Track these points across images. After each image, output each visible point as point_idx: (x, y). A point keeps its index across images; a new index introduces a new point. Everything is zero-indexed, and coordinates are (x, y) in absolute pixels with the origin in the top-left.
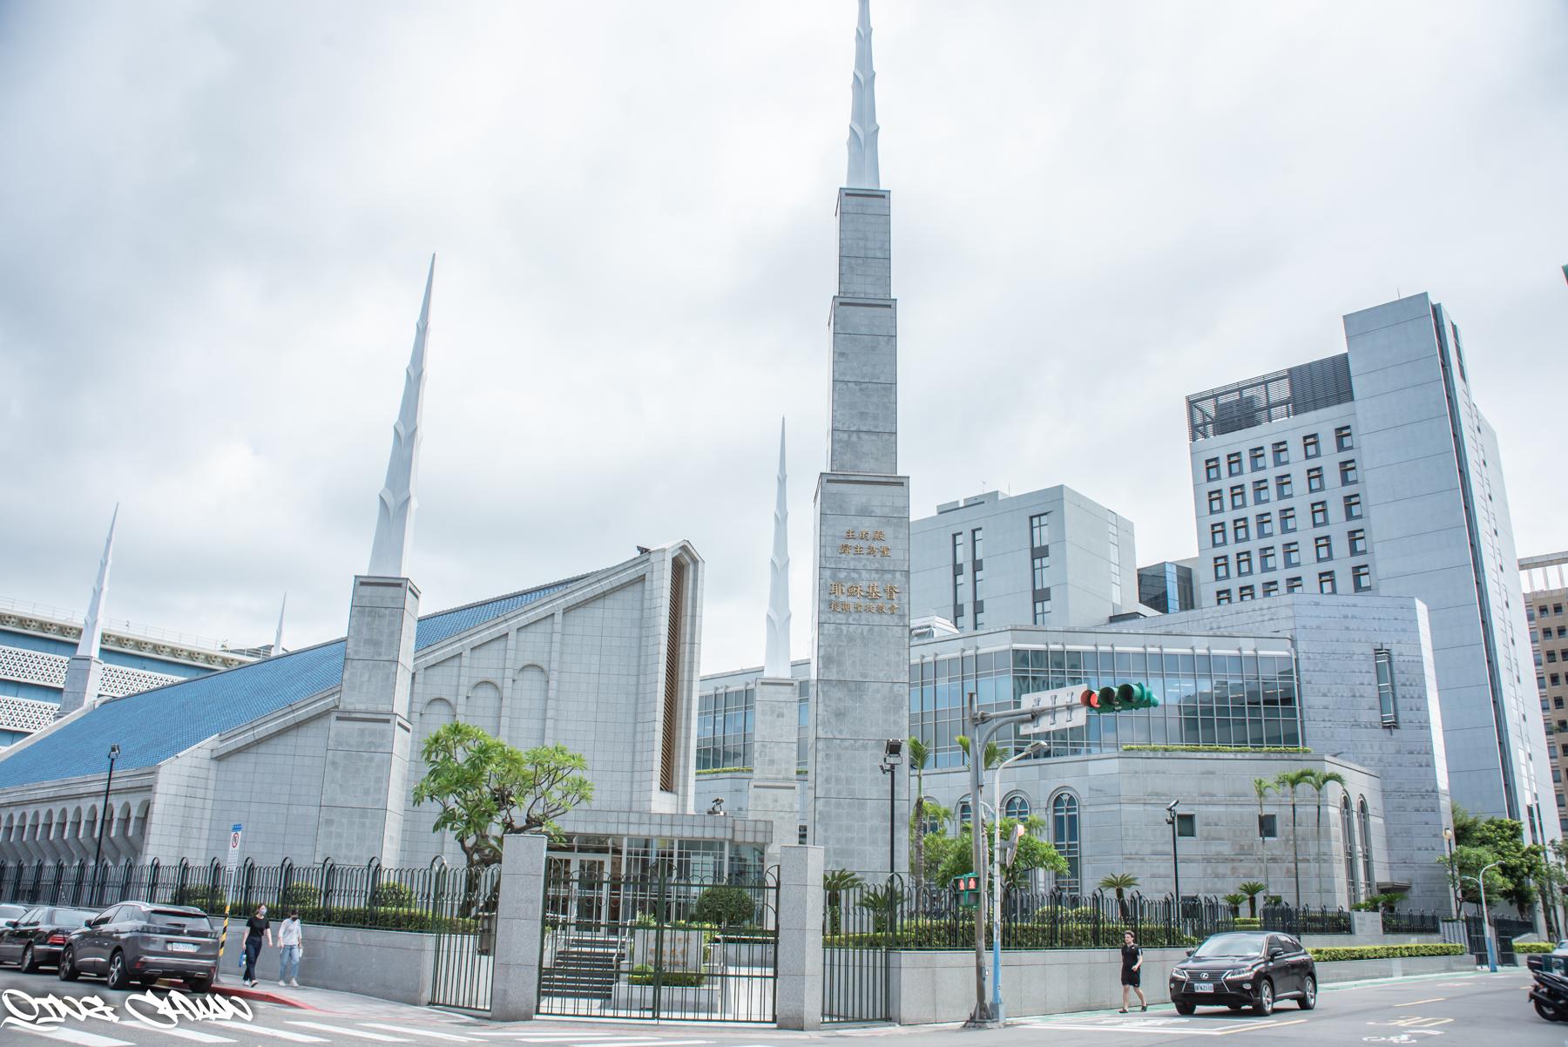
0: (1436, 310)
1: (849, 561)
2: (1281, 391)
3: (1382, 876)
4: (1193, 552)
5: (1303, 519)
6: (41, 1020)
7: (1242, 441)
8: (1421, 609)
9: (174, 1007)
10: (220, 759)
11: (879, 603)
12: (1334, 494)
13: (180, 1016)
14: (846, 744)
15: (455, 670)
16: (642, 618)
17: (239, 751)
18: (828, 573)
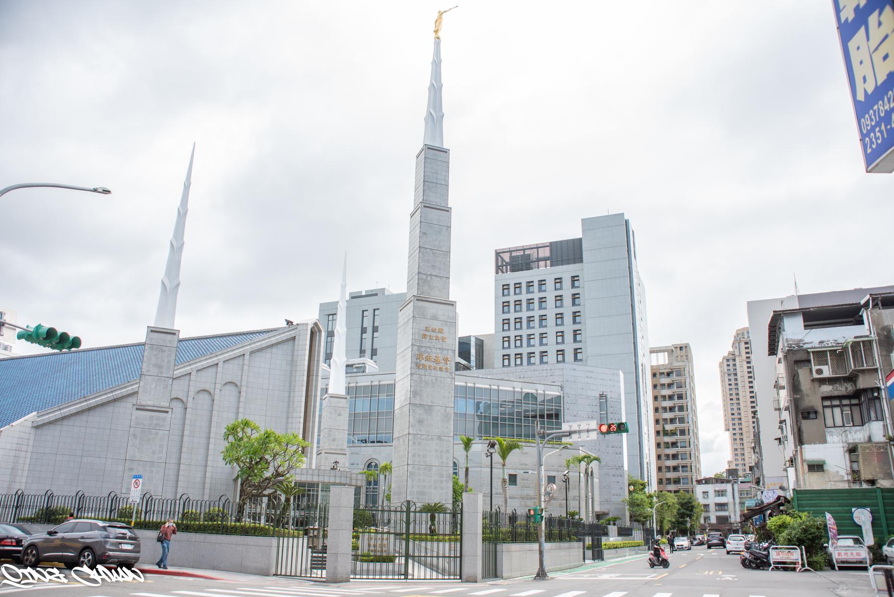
0: (627, 222)
1: (426, 343)
2: (546, 252)
3: (597, 509)
4: (492, 331)
5: (551, 320)
6: (23, 582)
7: (523, 277)
8: (621, 374)
9: (99, 574)
10: (37, 427)
11: (441, 365)
12: (568, 310)
13: (102, 579)
14: (424, 437)
15: (187, 382)
16: (292, 360)
17: (50, 423)
18: (416, 348)
